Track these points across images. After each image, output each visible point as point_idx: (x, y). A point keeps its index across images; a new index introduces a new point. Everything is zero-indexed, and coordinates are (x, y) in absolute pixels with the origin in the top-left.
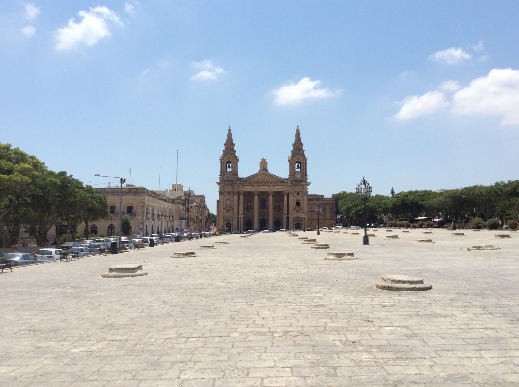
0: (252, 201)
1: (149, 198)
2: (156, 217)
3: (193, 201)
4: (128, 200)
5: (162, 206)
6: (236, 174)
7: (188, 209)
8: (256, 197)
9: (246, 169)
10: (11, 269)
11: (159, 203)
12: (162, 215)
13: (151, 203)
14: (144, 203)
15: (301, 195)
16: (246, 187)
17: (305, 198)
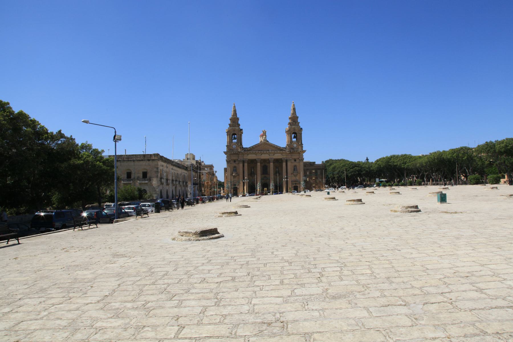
0: (255, 167)
1: (163, 163)
2: (170, 182)
3: (204, 169)
4: (144, 166)
5: (176, 172)
6: (241, 144)
7: (200, 176)
8: (259, 164)
9: (249, 141)
10: (18, 240)
11: (172, 169)
12: (176, 181)
13: (165, 169)
14: (157, 168)
15: (298, 161)
16: (250, 155)
17: (302, 164)
